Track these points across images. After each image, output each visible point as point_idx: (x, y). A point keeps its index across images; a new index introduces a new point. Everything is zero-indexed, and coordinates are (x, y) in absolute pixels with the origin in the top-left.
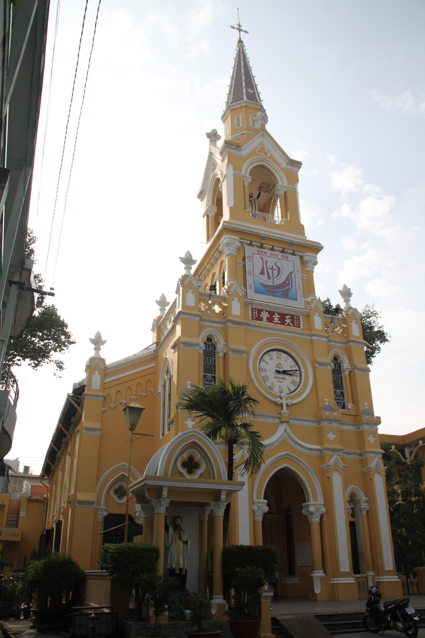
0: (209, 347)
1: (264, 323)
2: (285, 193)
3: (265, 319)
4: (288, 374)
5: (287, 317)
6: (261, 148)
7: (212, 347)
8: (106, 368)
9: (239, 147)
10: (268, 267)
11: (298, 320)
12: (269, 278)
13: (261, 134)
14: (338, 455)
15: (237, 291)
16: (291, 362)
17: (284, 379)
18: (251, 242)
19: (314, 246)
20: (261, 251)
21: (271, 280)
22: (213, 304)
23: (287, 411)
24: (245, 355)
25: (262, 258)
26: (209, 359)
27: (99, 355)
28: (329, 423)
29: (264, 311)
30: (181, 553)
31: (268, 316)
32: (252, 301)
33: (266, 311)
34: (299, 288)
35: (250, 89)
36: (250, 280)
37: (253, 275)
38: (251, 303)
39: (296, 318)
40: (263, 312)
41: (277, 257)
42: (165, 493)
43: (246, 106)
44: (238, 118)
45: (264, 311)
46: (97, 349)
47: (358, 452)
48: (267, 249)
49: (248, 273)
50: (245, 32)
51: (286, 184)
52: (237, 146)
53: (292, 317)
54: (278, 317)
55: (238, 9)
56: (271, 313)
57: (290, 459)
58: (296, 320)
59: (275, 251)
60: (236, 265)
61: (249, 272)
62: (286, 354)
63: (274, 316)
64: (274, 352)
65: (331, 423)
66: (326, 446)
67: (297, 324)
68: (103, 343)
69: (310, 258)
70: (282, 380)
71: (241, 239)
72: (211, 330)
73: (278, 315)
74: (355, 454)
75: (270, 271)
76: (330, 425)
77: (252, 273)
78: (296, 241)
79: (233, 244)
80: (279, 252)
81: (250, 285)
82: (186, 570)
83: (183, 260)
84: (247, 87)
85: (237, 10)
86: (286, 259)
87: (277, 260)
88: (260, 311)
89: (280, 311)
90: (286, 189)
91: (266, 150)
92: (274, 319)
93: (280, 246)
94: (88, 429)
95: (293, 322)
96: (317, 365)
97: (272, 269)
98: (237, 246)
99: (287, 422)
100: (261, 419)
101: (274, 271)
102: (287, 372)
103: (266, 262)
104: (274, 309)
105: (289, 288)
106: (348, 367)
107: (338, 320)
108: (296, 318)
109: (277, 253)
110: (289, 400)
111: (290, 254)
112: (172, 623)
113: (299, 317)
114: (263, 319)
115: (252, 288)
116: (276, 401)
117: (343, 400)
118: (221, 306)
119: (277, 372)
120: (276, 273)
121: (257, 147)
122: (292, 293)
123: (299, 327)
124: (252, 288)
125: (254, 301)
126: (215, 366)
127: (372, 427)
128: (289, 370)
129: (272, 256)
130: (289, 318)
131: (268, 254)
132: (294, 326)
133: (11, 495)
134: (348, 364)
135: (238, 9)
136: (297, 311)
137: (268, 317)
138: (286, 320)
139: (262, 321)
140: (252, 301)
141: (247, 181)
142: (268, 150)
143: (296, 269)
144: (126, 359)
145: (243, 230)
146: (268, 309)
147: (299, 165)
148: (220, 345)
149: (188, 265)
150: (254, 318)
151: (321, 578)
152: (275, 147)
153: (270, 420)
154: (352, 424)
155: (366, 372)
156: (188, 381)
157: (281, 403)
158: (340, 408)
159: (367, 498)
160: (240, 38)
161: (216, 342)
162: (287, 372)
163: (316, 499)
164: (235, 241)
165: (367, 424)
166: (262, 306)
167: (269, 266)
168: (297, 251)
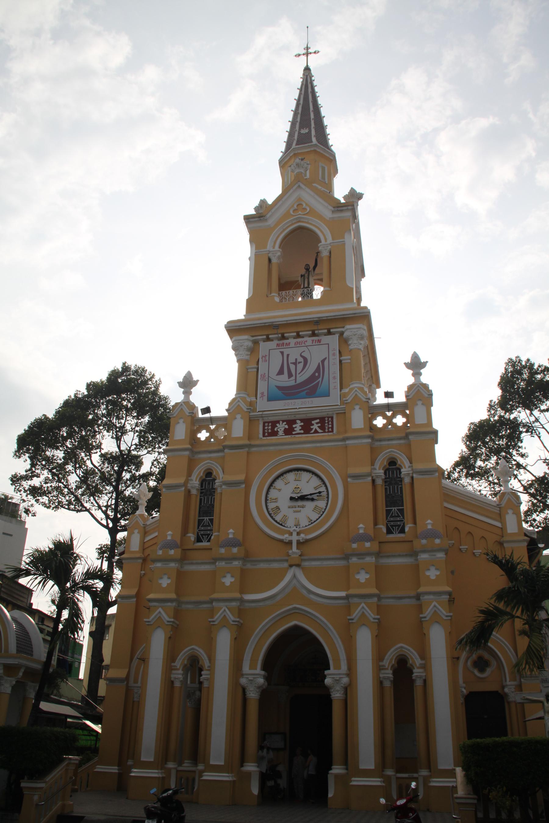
0: (393, 473)
1: (281, 437)
2: (330, 253)
3: (281, 433)
4: (308, 499)
5: (313, 422)
6: (298, 205)
7: (396, 472)
9: (262, 217)
10: (290, 362)
11: (330, 423)
12: (290, 375)
14: (365, 603)
15: (240, 406)
16: (315, 481)
17: (303, 507)
18: (268, 336)
19: (355, 314)
20: (282, 344)
21: (293, 378)
22: (394, 416)
23: (297, 551)
24: (244, 486)
25: (282, 353)
26: (208, 499)
28: (359, 559)
29: (281, 422)
31: (287, 427)
32: (261, 413)
33: (283, 421)
34: (334, 378)
35: (305, 129)
36: (262, 387)
37: (267, 379)
38: (261, 416)
40: (279, 424)
41: (304, 345)
43: (295, 154)
45: (281, 422)
47: (413, 593)
48: (292, 337)
49: (261, 378)
50: (299, 55)
52: (259, 217)
53: (322, 420)
54: (300, 426)
55: (308, 27)
57: (300, 613)
58: (328, 423)
59: (303, 337)
60: (248, 372)
61: (262, 376)
62: (308, 473)
63: (294, 426)
64: (290, 473)
65: (363, 559)
66: (352, 591)
67: (329, 428)
69: (351, 331)
70: (299, 509)
71: (253, 336)
72: (208, 463)
73: (301, 422)
74: (409, 597)
75: (292, 367)
76: (361, 561)
77: (267, 377)
78: (327, 316)
79: (241, 346)
80: (278, 340)
81: (262, 394)
85: (307, 28)
86: (319, 344)
88: (274, 424)
89: (303, 417)
90: (330, 247)
91: (304, 205)
92: (295, 429)
93: (306, 329)
95: (322, 428)
96: (349, 480)
97: (295, 364)
98: (246, 347)
99: (298, 565)
100: (262, 565)
101: (298, 365)
102: (306, 497)
103: (288, 355)
104: (293, 416)
105: (319, 381)
106: (409, 471)
107: (398, 407)
108: (328, 420)
109: (306, 339)
110: (302, 535)
111: (325, 335)
112: (53, 810)
113: (332, 418)
114: (279, 433)
115: (265, 396)
116: (283, 539)
117: (402, 521)
118: (404, 415)
119: (292, 499)
120: (300, 367)
121: (293, 206)
123: (332, 431)
124: (265, 396)
126: (213, 506)
127: (435, 555)
128: (309, 494)
129: (302, 345)
130: (317, 423)
132: (325, 432)
134: (409, 467)
135: (308, 27)
136: (327, 410)
137: (285, 428)
138: (312, 427)
139: (277, 436)
140: (261, 413)
141: (326, 250)
142: (306, 204)
145: (251, 325)
146: (285, 418)
148: (405, 468)
150: (266, 434)
151: (336, 776)
152: (283, 199)
153: (275, 565)
154: (406, 555)
155: (433, 474)
156: (359, 525)
157: (289, 540)
158: (206, 541)
159: (423, 662)
160: (307, 65)
161: (400, 465)
162: (306, 497)
163: (338, 667)
164: (244, 342)
165: (424, 551)
166: (300, 414)
167: (292, 360)
168: (332, 328)
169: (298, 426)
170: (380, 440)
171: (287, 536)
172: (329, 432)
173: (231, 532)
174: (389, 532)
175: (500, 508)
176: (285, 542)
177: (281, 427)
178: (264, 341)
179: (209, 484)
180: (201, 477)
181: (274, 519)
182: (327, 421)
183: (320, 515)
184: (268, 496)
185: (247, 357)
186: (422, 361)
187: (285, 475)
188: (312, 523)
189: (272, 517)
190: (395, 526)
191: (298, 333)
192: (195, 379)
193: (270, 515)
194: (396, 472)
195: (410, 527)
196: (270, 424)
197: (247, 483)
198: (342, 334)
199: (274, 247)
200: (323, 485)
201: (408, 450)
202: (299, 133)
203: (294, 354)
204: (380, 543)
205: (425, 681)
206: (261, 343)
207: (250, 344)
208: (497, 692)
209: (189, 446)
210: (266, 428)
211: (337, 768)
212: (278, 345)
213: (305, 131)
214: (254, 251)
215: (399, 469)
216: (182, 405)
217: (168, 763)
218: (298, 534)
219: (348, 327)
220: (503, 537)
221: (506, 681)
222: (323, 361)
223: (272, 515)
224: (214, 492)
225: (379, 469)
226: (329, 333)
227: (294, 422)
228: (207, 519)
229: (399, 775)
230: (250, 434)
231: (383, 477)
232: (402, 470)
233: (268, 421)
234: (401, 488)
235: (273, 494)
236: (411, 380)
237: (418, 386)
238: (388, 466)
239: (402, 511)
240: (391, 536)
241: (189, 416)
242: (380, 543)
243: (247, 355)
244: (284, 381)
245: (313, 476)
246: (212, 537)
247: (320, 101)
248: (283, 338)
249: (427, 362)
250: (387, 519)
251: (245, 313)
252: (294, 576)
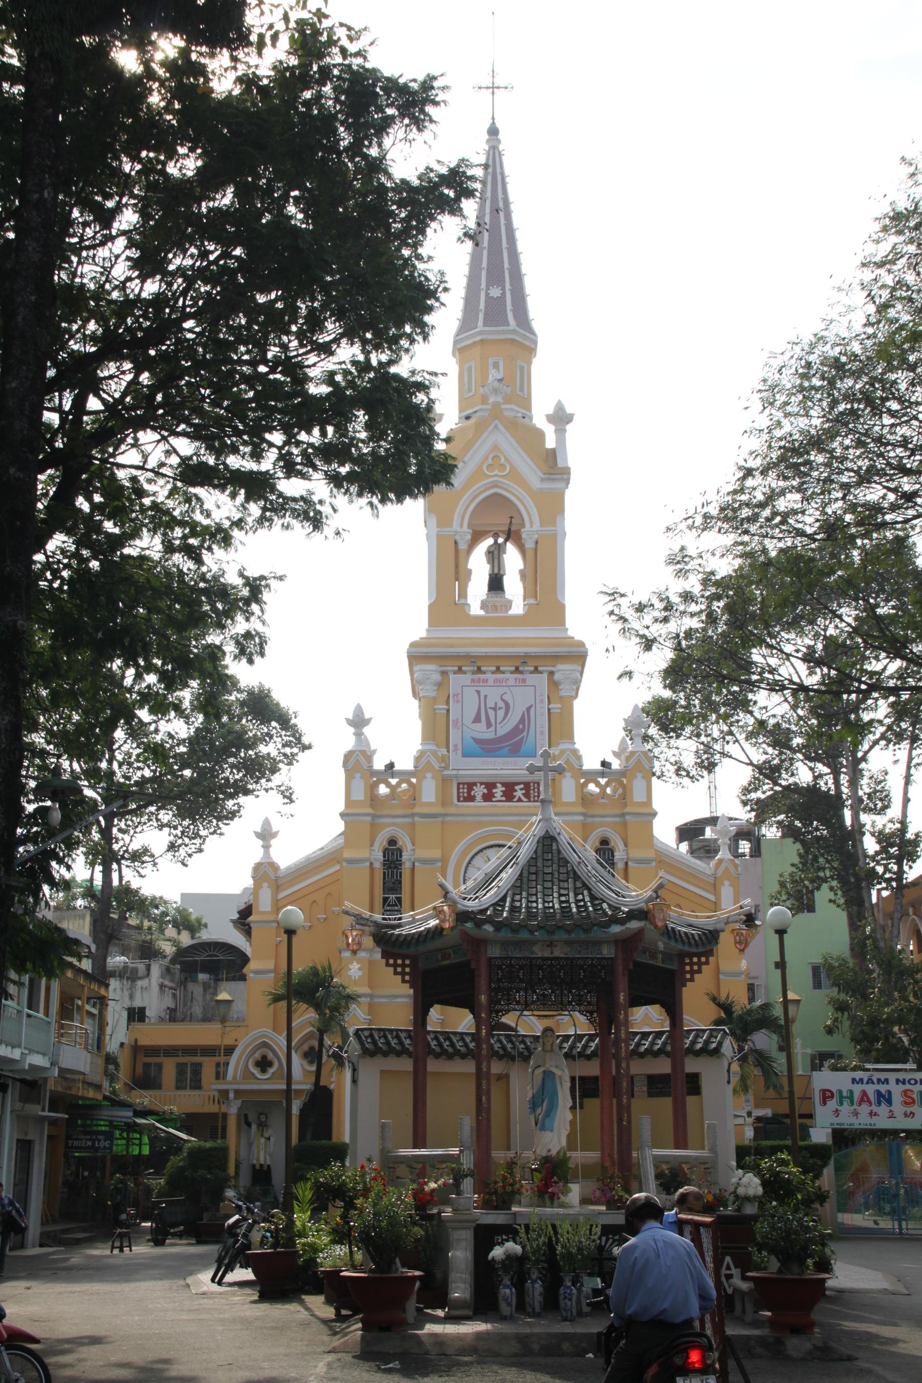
1: (479, 803)
2: (537, 542)
3: (479, 798)
5: (517, 788)
8: (277, 878)
10: (488, 705)
12: (489, 725)
13: (492, 426)
25: (478, 692)
27: (270, 857)
31: (485, 791)
33: (481, 784)
34: (542, 733)
36: (455, 737)
42: (231, 1095)
43: (482, 341)
44: (470, 369)
46: (266, 847)
51: (537, 526)
53: (527, 786)
56: (490, 786)
59: (503, 672)
68: (274, 835)
75: (491, 713)
81: (456, 746)
82: (269, 1166)
84: (489, 284)
87: (506, 689)
88: (471, 786)
91: (503, 460)
94: (257, 972)
95: (527, 795)
97: (495, 709)
103: (486, 696)
109: (507, 675)
111: (531, 673)
113: (538, 784)
120: (501, 713)
121: (486, 459)
122: (526, 747)
125: (461, 772)
126: (400, 883)
131: (491, 682)
133: (67, 1144)
140: (455, 772)
142: (506, 459)
143: (538, 699)
144: (307, 858)
147: (565, 476)
160: (493, 123)
167: (491, 704)
169: (499, 791)
170: (593, 816)
177: (479, 791)
178: (455, 673)
181: (476, 854)
185: (433, 694)
191: (498, 668)
197: (444, 861)
198: (551, 673)
199: (461, 525)
201: (623, 829)
202: (487, 295)
203: (493, 696)
206: (451, 676)
207: (437, 677)
212: (473, 681)
213: (495, 292)
214: (435, 530)
219: (560, 667)
222: (528, 709)
226: (536, 670)
228: (392, 897)
230: (444, 801)
239: (399, 900)
244: (482, 731)
247: (521, 246)
248: (479, 670)
251: (426, 626)
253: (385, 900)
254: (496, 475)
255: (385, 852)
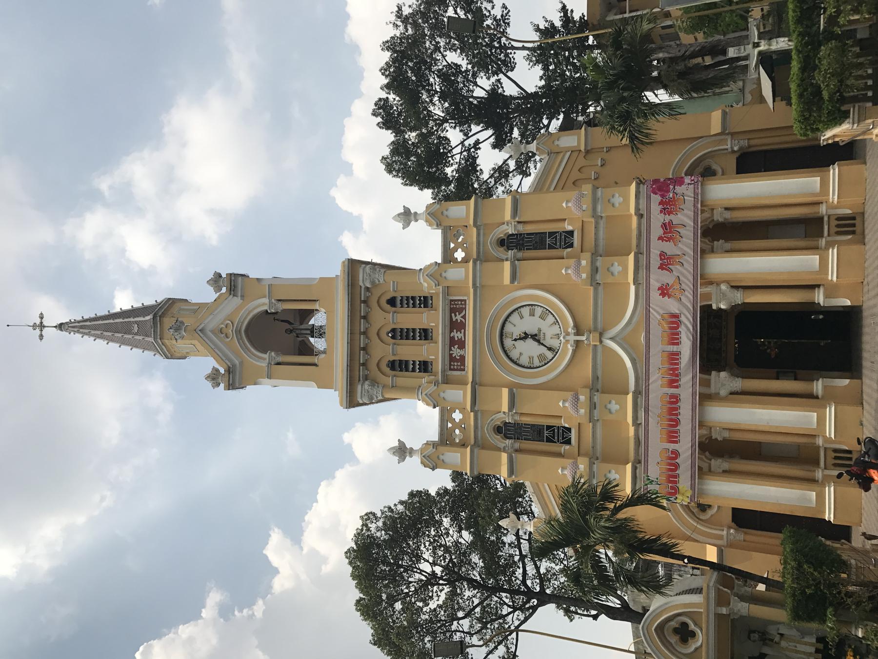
0: (511, 243)
3: (462, 352)
5: (454, 320)
7: (509, 426)
29: (451, 352)
30: (796, 647)
31: (456, 346)
33: (450, 350)
39: (453, 305)
43: (160, 339)
45: (451, 352)
53: (453, 311)
58: (456, 305)
62: (506, 325)
63: (456, 339)
67: (461, 304)
71: (359, 380)
83: (406, 224)
88: (452, 359)
92: (460, 338)
99: (601, 335)
108: (453, 305)
110: (570, 330)
113: (451, 301)
117: (561, 233)
123: (465, 301)
126: (533, 426)
130: (456, 316)
138: (459, 321)
146: (447, 347)
149: (412, 217)
151: (826, 296)
161: (505, 235)
169: (457, 335)
171: (569, 346)
172: (465, 304)
173: (563, 404)
174: (571, 246)
175: (551, 153)
176: (576, 347)
179: (509, 430)
180: (502, 437)
182: (455, 306)
183: (550, 313)
184: (526, 366)
186: (403, 211)
187: (506, 349)
188: (557, 321)
189: (548, 362)
190: (563, 435)
192: (396, 444)
193: (546, 364)
194: (509, 426)
195: (568, 225)
196: (452, 363)
198: (367, 289)
200: (519, 310)
204: (582, 252)
205: (726, 209)
208: (737, 159)
209: (469, 449)
210: (455, 367)
211: (818, 296)
215: (506, 423)
216: (424, 456)
217: (817, 479)
218: (568, 334)
220: (580, 150)
221: (727, 149)
223: (546, 362)
224: (518, 424)
225: (507, 255)
227: (452, 339)
228: (546, 433)
229: (826, 233)
231: (516, 250)
232: (510, 233)
233: (448, 365)
234: (528, 234)
235: (524, 360)
236: (422, 223)
237: (428, 214)
238: (505, 247)
239: (549, 427)
240: (575, 244)
241: (436, 449)
242: (582, 252)
243: (378, 387)
245: (508, 320)
246: (567, 426)
249: (404, 206)
250: (556, 442)
252: (612, 339)
253: (549, 440)
254: (232, 331)
255: (506, 437)
